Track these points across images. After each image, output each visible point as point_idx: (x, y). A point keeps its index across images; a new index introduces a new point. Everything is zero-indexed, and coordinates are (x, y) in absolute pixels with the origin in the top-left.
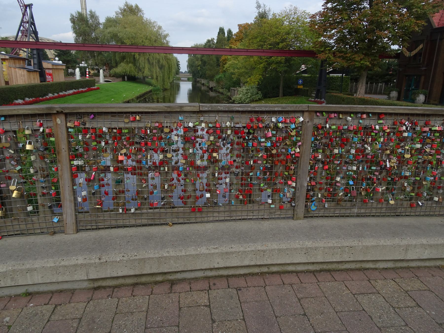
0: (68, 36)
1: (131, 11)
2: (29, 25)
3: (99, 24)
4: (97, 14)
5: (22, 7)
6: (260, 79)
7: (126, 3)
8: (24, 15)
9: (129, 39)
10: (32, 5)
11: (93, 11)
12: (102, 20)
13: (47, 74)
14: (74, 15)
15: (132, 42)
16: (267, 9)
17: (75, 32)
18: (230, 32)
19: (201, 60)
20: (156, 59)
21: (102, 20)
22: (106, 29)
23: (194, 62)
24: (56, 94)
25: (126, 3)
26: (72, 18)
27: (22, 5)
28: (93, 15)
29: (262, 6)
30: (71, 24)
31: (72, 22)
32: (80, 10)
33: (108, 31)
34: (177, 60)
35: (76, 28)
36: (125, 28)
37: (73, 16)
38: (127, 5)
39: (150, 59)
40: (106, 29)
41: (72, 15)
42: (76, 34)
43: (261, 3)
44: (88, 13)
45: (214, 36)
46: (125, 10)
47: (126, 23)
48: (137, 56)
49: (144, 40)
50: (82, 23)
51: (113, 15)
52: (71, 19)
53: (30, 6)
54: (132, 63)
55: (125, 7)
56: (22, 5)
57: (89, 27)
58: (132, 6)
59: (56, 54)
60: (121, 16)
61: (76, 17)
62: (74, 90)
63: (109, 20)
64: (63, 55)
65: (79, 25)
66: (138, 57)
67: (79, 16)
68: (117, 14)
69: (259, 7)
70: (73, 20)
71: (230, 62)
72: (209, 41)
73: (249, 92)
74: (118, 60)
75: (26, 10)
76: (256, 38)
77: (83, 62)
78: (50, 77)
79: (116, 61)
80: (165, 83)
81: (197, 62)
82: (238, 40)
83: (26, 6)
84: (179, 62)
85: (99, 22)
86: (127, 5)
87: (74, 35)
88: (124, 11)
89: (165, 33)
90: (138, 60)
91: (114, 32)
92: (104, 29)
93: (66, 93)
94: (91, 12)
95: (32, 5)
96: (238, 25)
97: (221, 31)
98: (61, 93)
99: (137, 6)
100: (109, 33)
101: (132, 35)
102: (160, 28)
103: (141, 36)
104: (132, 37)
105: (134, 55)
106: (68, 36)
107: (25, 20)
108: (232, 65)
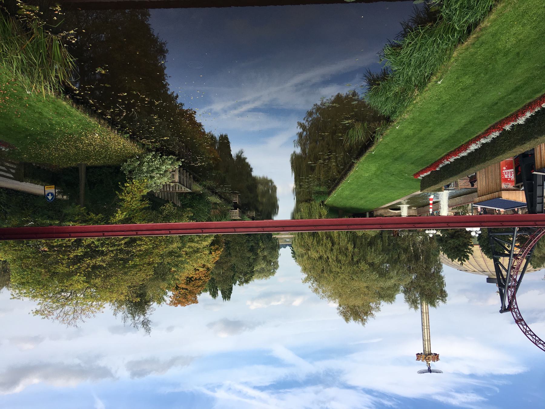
0: (450, 271)
1: (356, 312)
2: (505, 284)
3: (405, 292)
4: (407, 306)
5: (516, 307)
6: (121, 191)
7: (364, 324)
8: (514, 296)
9: (362, 271)
10: (501, 312)
11: (413, 309)
12: (400, 297)
13: (510, 181)
14: (440, 303)
15: (358, 267)
16: (130, 321)
17: (440, 278)
18: (214, 295)
19: (257, 254)
20: (322, 245)
21: (400, 297)
22: (395, 285)
23: (270, 253)
24: (507, 127)
25: (364, 324)
26: (443, 297)
27: (516, 310)
28: (414, 303)
29: (140, 326)
30: (446, 289)
31: (445, 292)
32: (431, 309)
33: (393, 281)
34: (296, 259)
35: (439, 284)
36: (367, 287)
37: (442, 300)
38: (363, 321)
39: (330, 244)
40: (395, 285)
41: (444, 301)
42: (440, 276)
43: (142, 330)
44: (419, 306)
45: (237, 289)
46: (366, 314)
47: (365, 294)
48: (350, 247)
49: (338, 270)
50: (428, 290)
51: (384, 305)
52: (446, 296)
53: (503, 310)
54: (357, 237)
55: (365, 318)
56: (516, 310)
57: (420, 286)
58: (354, 319)
59: (469, 247)
60: (373, 305)
61: (438, 299)
62: (464, 154)
63: (390, 297)
64: (459, 245)
65: (435, 288)
66: (349, 245)
67: (434, 302)
68: (378, 308)
69: (145, 324)
70: (443, 295)
71: (205, 243)
72: (247, 281)
73: (147, 172)
74: (379, 241)
75: (510, 303)
76: (135, 266)
77: (431, 236)
78: (506, 176)
79: (382, 240)
80: (307, 211)
81: (266, 254)
82: (196, 279)
83: (509, 309)
84: (293, 257)
85: (406, 294)
86: (363, 321)
87: (442, 274)
88: (367, 313)
89: (309, 284)
90: (349, 241)
91: (384, 279)
92: (399, 285)
93: (483, 141)
94: (416, 308)
95: (501, 312)
96: (197, 302)
97: (227, 295)
98: (495, 134)
99: (347, 320)
100: (392, 278)
101: (357, 276)
102: (316, 290)
103: (344, 276)
104: (357, 273)
105: (354, 247)
106: (450, 271)
107: (513, 289)
108: (201, 240)
